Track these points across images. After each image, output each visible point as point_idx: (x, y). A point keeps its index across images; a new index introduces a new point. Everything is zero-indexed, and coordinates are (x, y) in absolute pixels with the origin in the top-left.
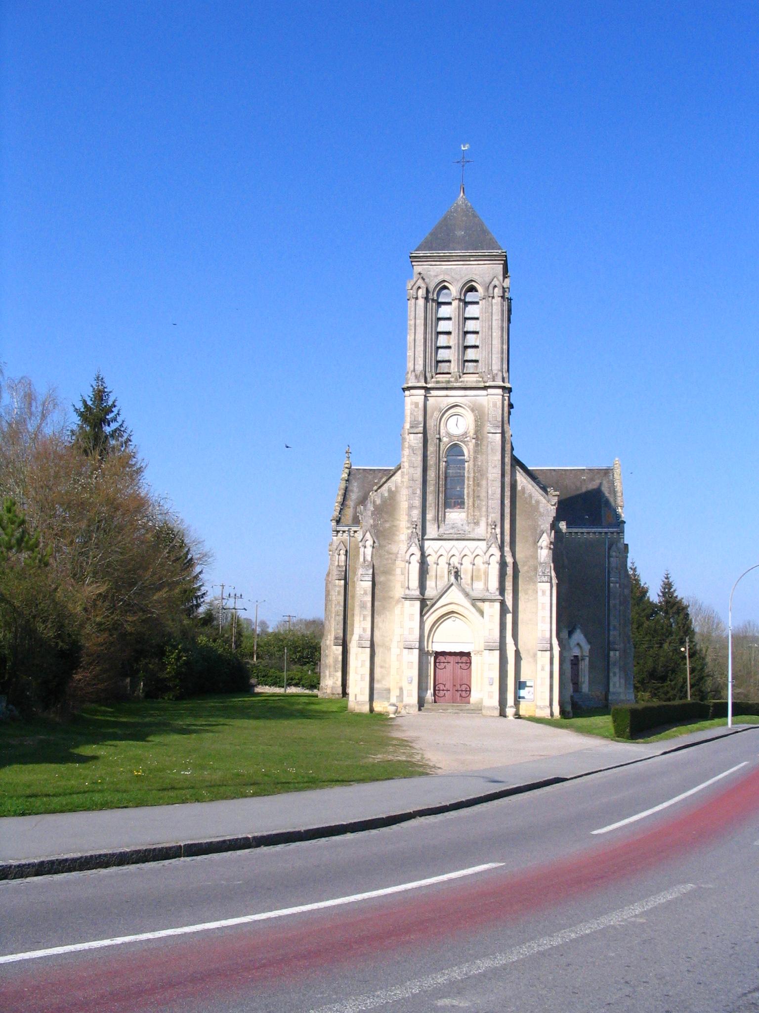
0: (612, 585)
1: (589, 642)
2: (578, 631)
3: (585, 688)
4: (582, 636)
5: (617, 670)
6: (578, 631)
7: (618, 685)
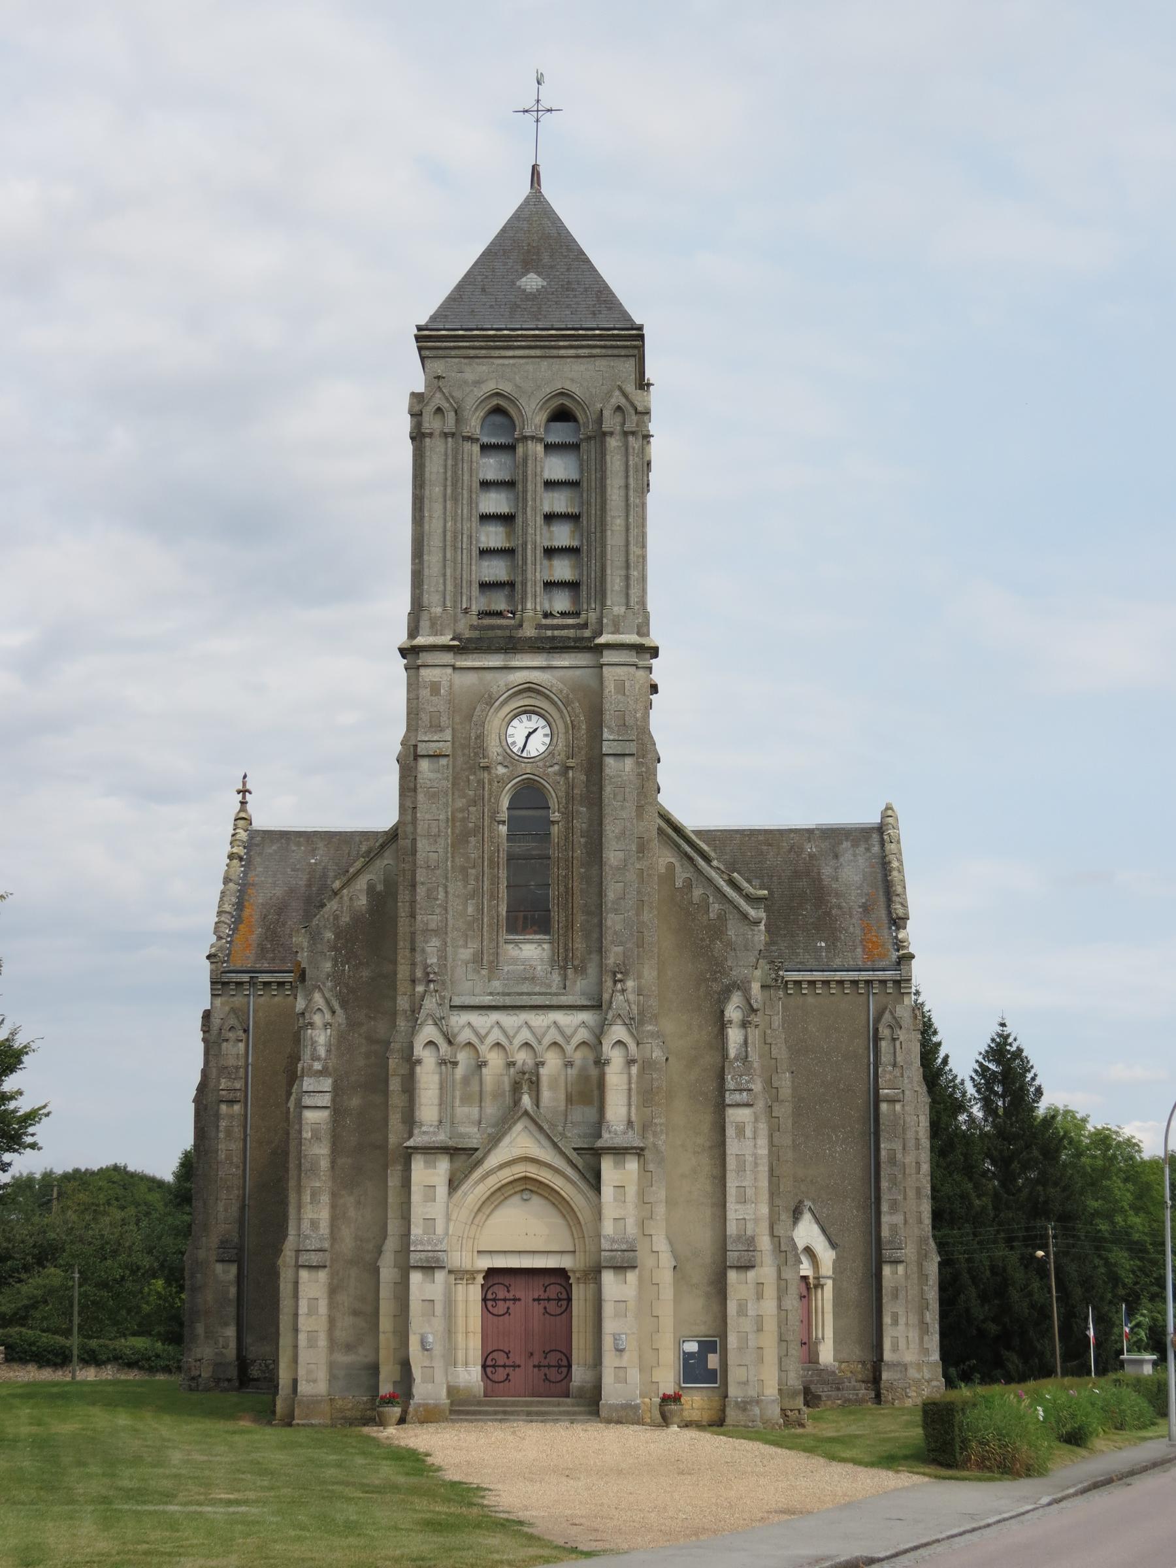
0: (884, 1107)
1: (833, 1245)
2: (807, 1217)
3: (827, 1354)
4: (816, 1229)
5: (901, 1311)
6: (807, 1217)
7: (902, 1344)
